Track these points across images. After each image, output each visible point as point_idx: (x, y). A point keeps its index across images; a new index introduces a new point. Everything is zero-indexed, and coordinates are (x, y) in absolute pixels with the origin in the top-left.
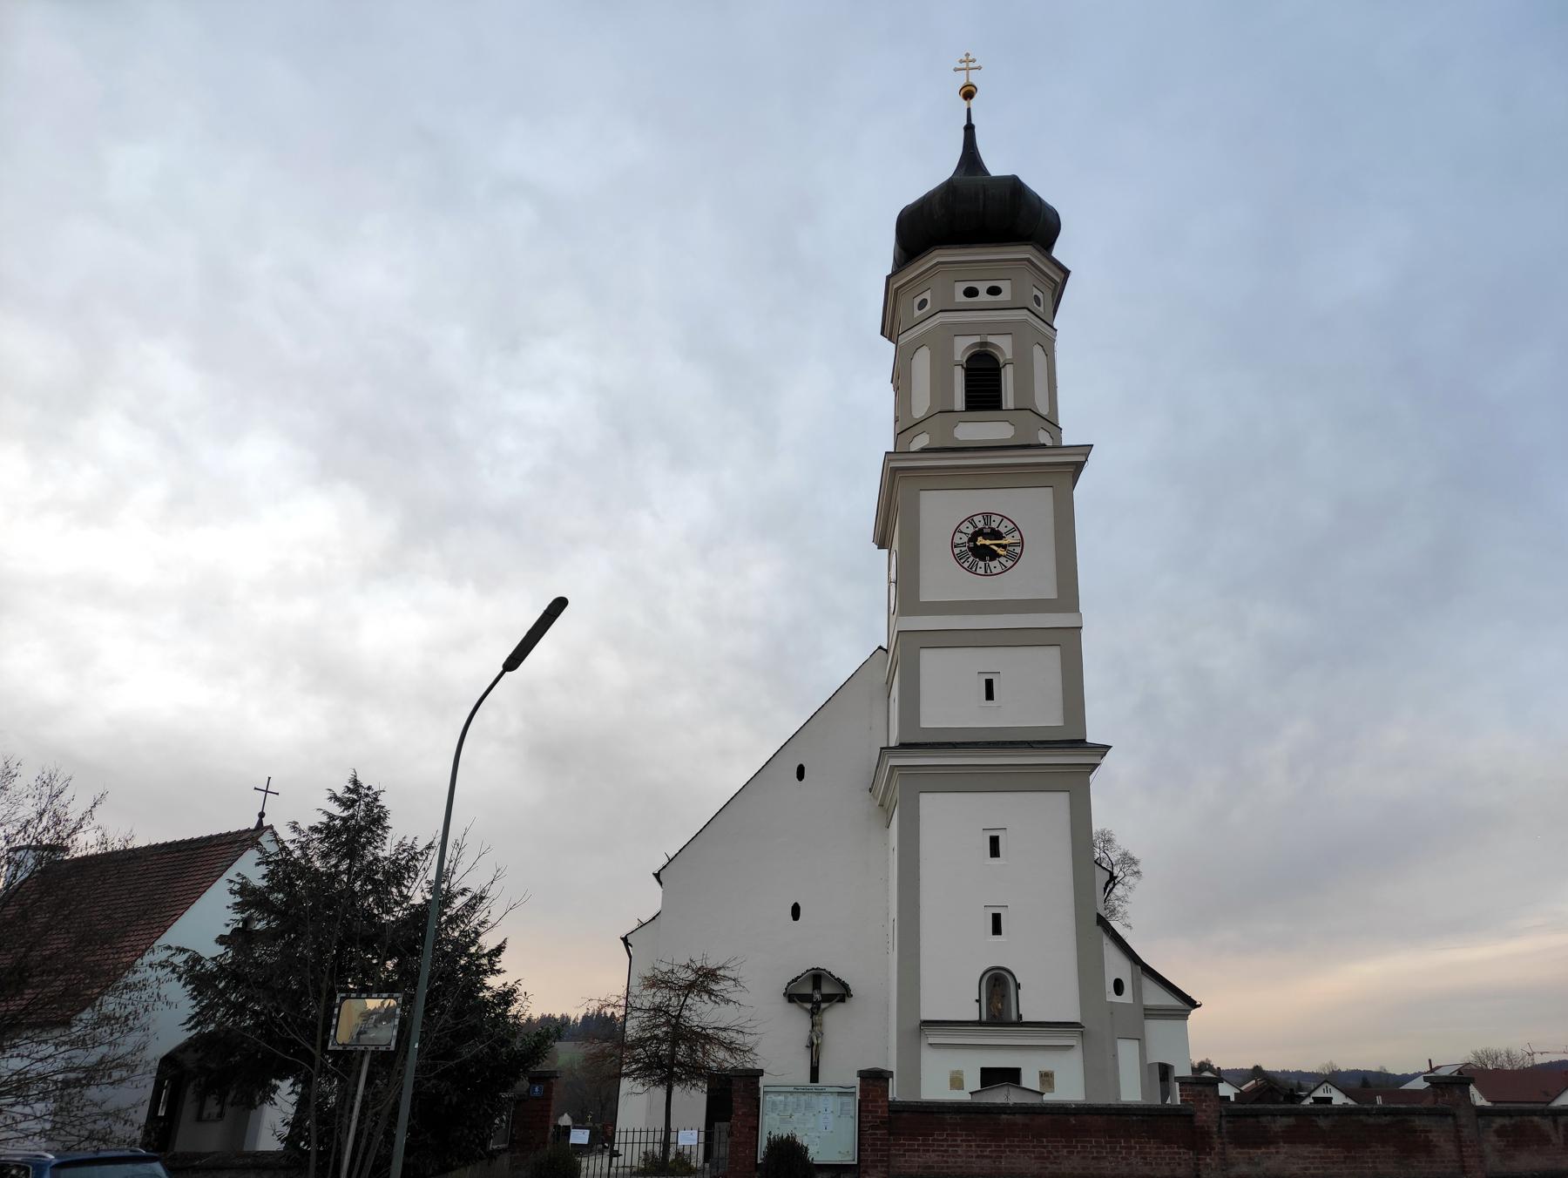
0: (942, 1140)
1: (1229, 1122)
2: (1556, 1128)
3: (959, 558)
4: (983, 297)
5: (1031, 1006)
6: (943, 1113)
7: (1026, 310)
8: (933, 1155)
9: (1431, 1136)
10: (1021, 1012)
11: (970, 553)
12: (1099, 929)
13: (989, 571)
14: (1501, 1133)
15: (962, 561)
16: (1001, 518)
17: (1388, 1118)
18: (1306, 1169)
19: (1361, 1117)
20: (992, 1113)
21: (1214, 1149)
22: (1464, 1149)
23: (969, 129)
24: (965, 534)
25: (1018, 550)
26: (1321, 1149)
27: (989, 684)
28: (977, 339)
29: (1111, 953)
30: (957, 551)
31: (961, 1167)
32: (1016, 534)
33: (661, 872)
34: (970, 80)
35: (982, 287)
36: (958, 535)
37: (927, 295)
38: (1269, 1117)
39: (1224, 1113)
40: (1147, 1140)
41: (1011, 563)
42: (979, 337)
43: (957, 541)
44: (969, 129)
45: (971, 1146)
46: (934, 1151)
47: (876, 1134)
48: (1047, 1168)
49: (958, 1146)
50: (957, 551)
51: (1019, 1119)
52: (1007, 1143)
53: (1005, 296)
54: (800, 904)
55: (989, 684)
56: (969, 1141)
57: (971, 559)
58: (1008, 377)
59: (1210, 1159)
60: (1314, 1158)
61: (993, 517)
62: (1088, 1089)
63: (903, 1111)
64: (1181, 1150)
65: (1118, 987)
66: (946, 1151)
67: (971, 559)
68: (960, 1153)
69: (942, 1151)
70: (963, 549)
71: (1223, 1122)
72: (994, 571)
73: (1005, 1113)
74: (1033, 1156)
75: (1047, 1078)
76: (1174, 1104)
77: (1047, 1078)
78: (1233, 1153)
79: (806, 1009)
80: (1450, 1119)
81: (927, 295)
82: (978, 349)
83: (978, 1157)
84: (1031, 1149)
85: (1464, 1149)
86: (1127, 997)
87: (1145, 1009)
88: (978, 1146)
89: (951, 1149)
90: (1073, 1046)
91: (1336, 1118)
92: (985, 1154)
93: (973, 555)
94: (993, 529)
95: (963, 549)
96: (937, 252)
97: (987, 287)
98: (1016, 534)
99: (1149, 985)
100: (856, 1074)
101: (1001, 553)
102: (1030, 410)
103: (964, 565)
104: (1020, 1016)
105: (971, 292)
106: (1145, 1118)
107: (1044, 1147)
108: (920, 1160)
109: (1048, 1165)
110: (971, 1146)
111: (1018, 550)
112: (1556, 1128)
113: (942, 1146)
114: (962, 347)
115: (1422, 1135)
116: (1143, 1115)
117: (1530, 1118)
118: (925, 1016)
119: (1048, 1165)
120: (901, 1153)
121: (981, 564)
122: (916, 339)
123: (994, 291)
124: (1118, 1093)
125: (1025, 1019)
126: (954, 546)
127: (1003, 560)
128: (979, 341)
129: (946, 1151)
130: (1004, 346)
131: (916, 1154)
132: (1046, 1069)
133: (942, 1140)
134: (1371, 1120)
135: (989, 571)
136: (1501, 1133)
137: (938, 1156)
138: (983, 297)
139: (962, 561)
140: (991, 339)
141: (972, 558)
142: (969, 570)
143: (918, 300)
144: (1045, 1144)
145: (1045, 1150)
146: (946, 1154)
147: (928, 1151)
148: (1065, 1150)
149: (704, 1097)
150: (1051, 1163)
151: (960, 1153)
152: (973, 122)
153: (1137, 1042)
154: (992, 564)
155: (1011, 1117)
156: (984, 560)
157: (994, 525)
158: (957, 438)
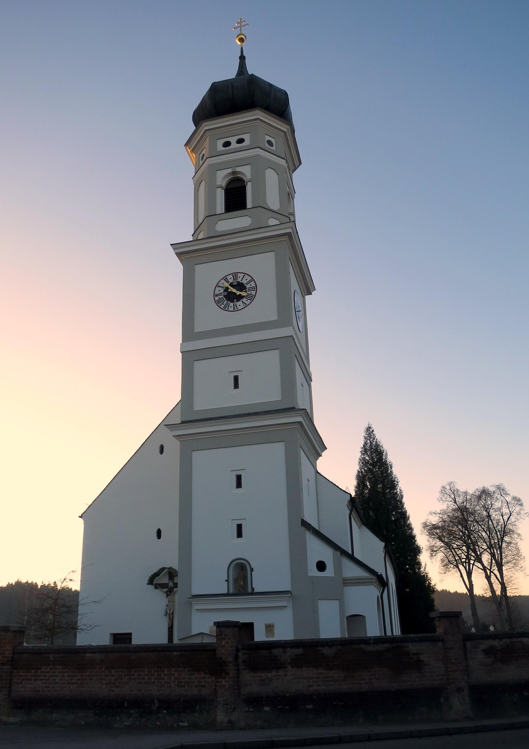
0: (47, 672)
1: (244, 654)
3: (218, 303)
4: (234, 145)
6: (49, 653)
7: (258, 149)
8: (40, 682)
9: (422, 657)
10: (253, 587)
11: (225, 299)
12: (303, 528)
13: (236, 308)
14: (487, 652)
15: (220, 304)
16: (243, 274)
17: (386, 645)
18: (311, 686)
20: (79, 653)
21: (228, 674)
22: (449, 666)
23: (242, 58)
24: (220, 287)
25: (253, 293)
26: (324, 671)
27: (236, 379)
28: (230, 170)
29: (312, 541)
30: (217, 298)
31: (56, 691)
32: (253, 282)
33: (83, 515)
35: (233, 140)
36: (218, 289)
37: (246, 137)
38: (281, 650)
39: (240, 647)
40: (182, 669)
41: (249, 301)
42: (231, 169)
43: (217, 292)
44: (242, 58)
45: (64, 676)
46: (41, 680)
47: (3, 669)
48: (113, 691)
49: (56, 676)
50: (217, 298)
51: (97, 656)
52: (88, 673)
53: (246, 143)
54: (161, 529)
55: (236, 379)
56: (64, 673)
57: (225, 303)
59: (225, 681)
60: (318, 678)
61: (239, 275)
62: (341, 636)
63: (24, 653)
64: (207, 676)
65: (321, 566)
66: (48, 680)
67: (225, 303)
68: (57, 681)
69: (45, 680)
70: (221, 297)
71: (240, 654)
72: (239, 308)
73: (89, 653)
74: (104, 682)
75: (270, 628)
76: (358, 635)
77: (270, 628)
78: (247, 676)
79: (164, 592)
80: (440, 644)
83: (68, 683)
84: (104, 677)
85: (449, 666)
86: (329, 572)
87: (344, 580)
88: (69, 676)
89: (52, 678)
90: (286, 606)
91: (339, 647)
92: (73, 681)
94: (238, 282)
95: (221, 297)
96: (204, 124)
97: (244, 142)
98: (253, 282)
99: (347, 564)
102: (260, 207)
103: (221, 307)
104: (253, 589)
105: (227, 144)
106: (183, 653)
107: (113, 676)
108: (31, 686)
109: (114, 689)
110: (64, 676)
111: (253, 293)
113: (46, 676)
115: (415, 656)
116: (181, 651)
117: (520, 639)
118: (195, 592)
119: (114, 689)
120: (20, 681)
121: (231, 304)
123: (241, 141)
124: (367, 635)
125: (256, 591)
127: (244, 300)
129: (48, 680)
130: (246, 172)
131: (29, 682)
132: (269, 622)
133: (47, 672)
134: (370, 648)
135: (236, 308)
136: (487, 652)
137: (43, 683)
139: (220, 304)
140: (238, 169)
141: (226, 301)
142: (224, 309)
143: (268, 138)
144: (113, 673)
145: (113, 678)
146: (48, 682)
147: (37, 680)
148: (127, 678)
150: (116, 687)
151: (57, 681)
153: (338, 601)
155: (93, 655)
156: (233, 301)
157: (239, 280)
158: (217, 231)
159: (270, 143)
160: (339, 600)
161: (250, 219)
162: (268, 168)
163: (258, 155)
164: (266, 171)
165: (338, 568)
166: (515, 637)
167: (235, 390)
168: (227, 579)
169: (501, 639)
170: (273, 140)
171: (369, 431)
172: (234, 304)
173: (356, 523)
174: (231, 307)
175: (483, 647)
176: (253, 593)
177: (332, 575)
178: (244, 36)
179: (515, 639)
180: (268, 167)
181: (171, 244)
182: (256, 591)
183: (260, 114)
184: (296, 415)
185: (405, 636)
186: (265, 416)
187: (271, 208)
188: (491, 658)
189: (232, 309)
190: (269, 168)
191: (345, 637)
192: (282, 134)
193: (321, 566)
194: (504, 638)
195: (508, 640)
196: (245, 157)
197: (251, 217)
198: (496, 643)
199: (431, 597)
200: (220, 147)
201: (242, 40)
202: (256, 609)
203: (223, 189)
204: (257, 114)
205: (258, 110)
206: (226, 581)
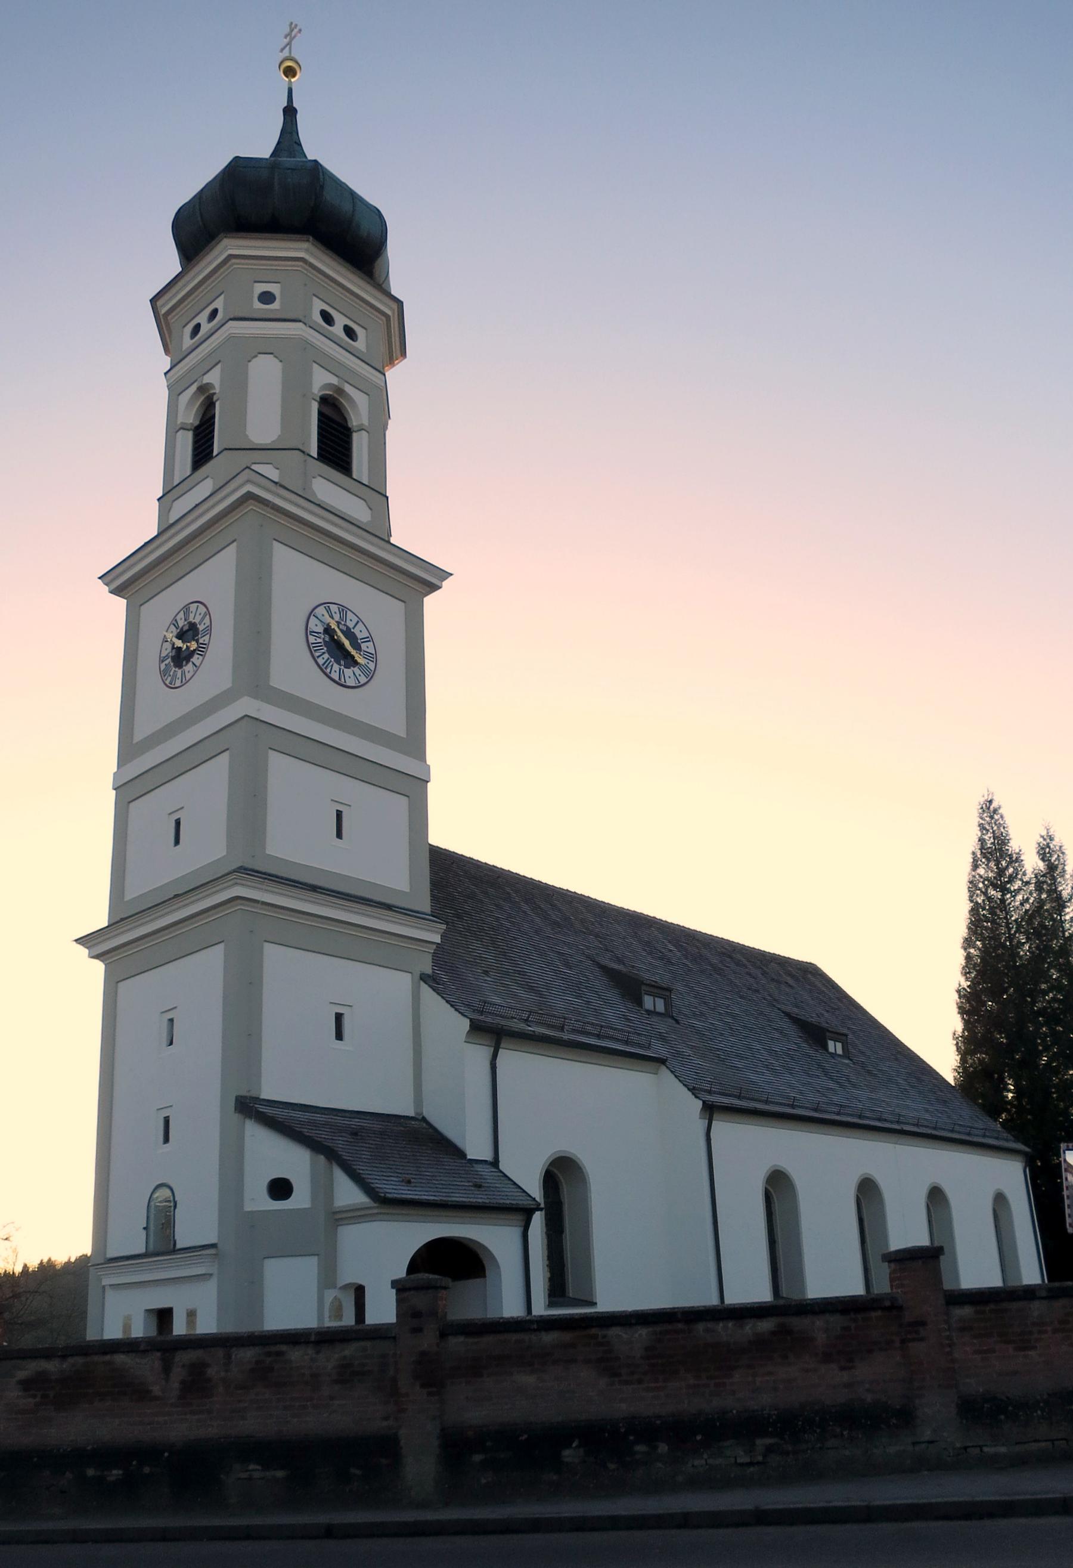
2: (167, 1369)
5: (184, 1237)
15: (317, 654)
19: (594, 1331)
23: (290, 112)
28: (334, 380)
34: (292, 55)
35: (340, 321)
37: (219, 304)
44: (290, 112)
53: (360, 344)
58: (360, 445)
75: (191, 1315)
76: (1012, 1283)
77: (191, 1315)
81: (219, 304)
82: (331, 393)
86: (300, 1199)
93: (329, 652)
96: (305, 245)
100: (390, 1286)
101: (359, 660)
112: (167, 1369)
114: (321, 380)
117: (108, 1358)
122: (265, 338)
126: (308, 632)
128: (336, 383)
130: (213, 378)
136: (27, 1385)
138: (338, 330)
140: (348, 388)
141: (326, 656)
143: (260, 288)
149: (184, 1333)
152: (295, 105)
154: (348, 672)
159: (267, 298)
160: (318, 1255)
161: (277, 471)
162: (256, 356)
163: (231, 337)
164: (250, 364)
165: (323, 1190)
166: (96, 1354)
167: (176, 847)
168: (145, 1226)
169: (64, 1357)
170: (274, 288)
171: (989, 810)
172: (362, 642)
173: (599, 1065)
174: (368, 647)
175: (22, 1375)
176: (174, 1251)
177: (307, 1204)
178: (294, 63)
179: (96, 1358)
180: (256, 354)
181: (100, 578)
182: (178, 1246)
183: (231, 246)
184: (226, 885)
185: (1057, 1284)
186: (198, 892)
187: (256, 442)
188: (35, 1396)
189: (321, 661)
190: (259, 355)
191: (323, 1326)
192: (298, 266)
193: (280, 1189)
194: (72, 1355)
195: (80, 1360)
196: (266, 336)
197: (278, 469)
198: (51, 1366)
199: (59, 1270)
200: (187, 342)
201: (290, 72)
202: (195, 1278)
203: (188, 430)
204: (227, 246)
205: (225, 237)
206: (144, 1228)
